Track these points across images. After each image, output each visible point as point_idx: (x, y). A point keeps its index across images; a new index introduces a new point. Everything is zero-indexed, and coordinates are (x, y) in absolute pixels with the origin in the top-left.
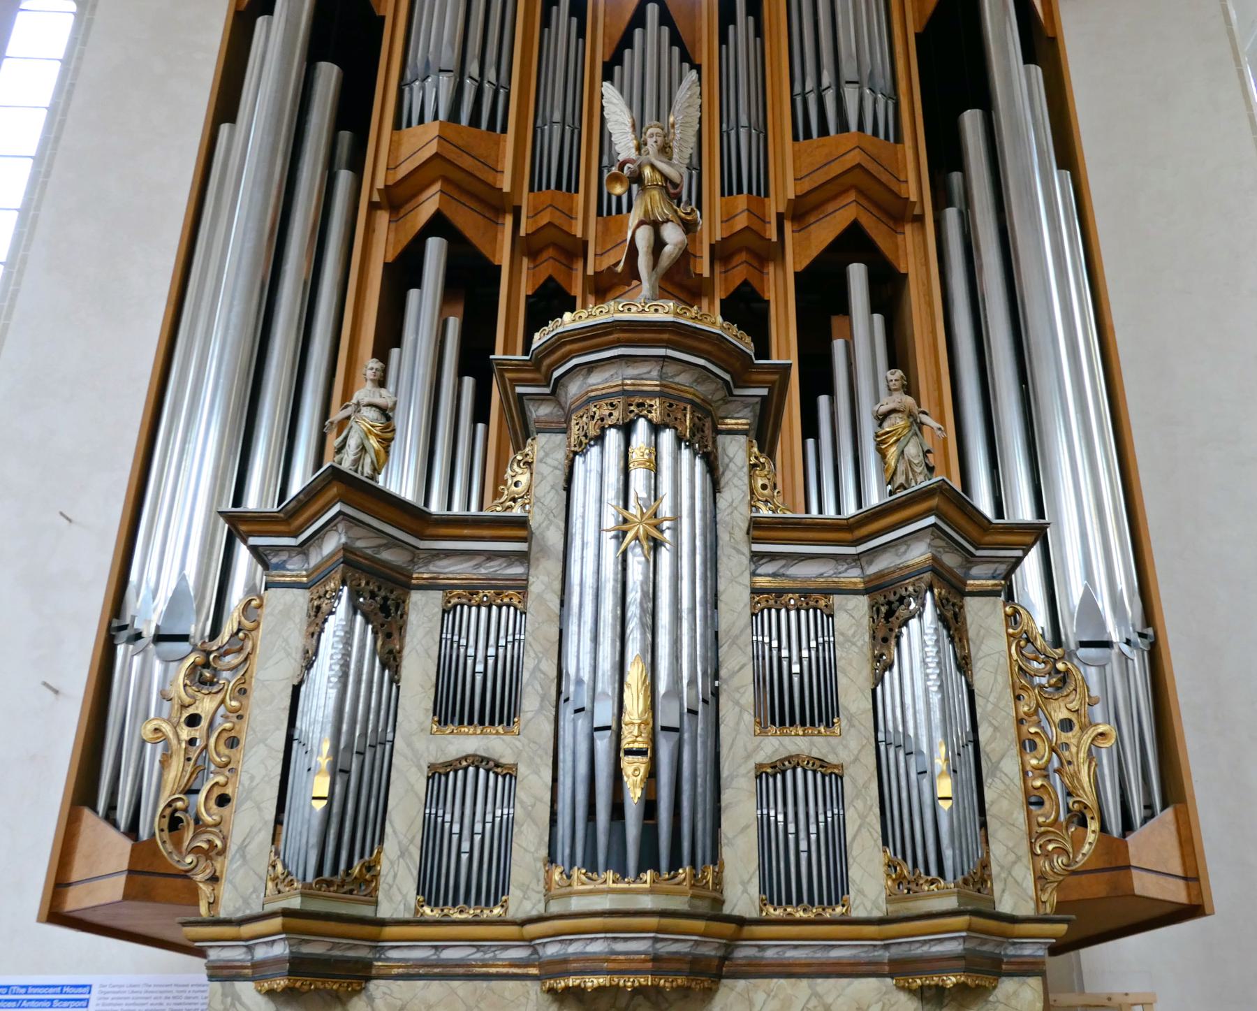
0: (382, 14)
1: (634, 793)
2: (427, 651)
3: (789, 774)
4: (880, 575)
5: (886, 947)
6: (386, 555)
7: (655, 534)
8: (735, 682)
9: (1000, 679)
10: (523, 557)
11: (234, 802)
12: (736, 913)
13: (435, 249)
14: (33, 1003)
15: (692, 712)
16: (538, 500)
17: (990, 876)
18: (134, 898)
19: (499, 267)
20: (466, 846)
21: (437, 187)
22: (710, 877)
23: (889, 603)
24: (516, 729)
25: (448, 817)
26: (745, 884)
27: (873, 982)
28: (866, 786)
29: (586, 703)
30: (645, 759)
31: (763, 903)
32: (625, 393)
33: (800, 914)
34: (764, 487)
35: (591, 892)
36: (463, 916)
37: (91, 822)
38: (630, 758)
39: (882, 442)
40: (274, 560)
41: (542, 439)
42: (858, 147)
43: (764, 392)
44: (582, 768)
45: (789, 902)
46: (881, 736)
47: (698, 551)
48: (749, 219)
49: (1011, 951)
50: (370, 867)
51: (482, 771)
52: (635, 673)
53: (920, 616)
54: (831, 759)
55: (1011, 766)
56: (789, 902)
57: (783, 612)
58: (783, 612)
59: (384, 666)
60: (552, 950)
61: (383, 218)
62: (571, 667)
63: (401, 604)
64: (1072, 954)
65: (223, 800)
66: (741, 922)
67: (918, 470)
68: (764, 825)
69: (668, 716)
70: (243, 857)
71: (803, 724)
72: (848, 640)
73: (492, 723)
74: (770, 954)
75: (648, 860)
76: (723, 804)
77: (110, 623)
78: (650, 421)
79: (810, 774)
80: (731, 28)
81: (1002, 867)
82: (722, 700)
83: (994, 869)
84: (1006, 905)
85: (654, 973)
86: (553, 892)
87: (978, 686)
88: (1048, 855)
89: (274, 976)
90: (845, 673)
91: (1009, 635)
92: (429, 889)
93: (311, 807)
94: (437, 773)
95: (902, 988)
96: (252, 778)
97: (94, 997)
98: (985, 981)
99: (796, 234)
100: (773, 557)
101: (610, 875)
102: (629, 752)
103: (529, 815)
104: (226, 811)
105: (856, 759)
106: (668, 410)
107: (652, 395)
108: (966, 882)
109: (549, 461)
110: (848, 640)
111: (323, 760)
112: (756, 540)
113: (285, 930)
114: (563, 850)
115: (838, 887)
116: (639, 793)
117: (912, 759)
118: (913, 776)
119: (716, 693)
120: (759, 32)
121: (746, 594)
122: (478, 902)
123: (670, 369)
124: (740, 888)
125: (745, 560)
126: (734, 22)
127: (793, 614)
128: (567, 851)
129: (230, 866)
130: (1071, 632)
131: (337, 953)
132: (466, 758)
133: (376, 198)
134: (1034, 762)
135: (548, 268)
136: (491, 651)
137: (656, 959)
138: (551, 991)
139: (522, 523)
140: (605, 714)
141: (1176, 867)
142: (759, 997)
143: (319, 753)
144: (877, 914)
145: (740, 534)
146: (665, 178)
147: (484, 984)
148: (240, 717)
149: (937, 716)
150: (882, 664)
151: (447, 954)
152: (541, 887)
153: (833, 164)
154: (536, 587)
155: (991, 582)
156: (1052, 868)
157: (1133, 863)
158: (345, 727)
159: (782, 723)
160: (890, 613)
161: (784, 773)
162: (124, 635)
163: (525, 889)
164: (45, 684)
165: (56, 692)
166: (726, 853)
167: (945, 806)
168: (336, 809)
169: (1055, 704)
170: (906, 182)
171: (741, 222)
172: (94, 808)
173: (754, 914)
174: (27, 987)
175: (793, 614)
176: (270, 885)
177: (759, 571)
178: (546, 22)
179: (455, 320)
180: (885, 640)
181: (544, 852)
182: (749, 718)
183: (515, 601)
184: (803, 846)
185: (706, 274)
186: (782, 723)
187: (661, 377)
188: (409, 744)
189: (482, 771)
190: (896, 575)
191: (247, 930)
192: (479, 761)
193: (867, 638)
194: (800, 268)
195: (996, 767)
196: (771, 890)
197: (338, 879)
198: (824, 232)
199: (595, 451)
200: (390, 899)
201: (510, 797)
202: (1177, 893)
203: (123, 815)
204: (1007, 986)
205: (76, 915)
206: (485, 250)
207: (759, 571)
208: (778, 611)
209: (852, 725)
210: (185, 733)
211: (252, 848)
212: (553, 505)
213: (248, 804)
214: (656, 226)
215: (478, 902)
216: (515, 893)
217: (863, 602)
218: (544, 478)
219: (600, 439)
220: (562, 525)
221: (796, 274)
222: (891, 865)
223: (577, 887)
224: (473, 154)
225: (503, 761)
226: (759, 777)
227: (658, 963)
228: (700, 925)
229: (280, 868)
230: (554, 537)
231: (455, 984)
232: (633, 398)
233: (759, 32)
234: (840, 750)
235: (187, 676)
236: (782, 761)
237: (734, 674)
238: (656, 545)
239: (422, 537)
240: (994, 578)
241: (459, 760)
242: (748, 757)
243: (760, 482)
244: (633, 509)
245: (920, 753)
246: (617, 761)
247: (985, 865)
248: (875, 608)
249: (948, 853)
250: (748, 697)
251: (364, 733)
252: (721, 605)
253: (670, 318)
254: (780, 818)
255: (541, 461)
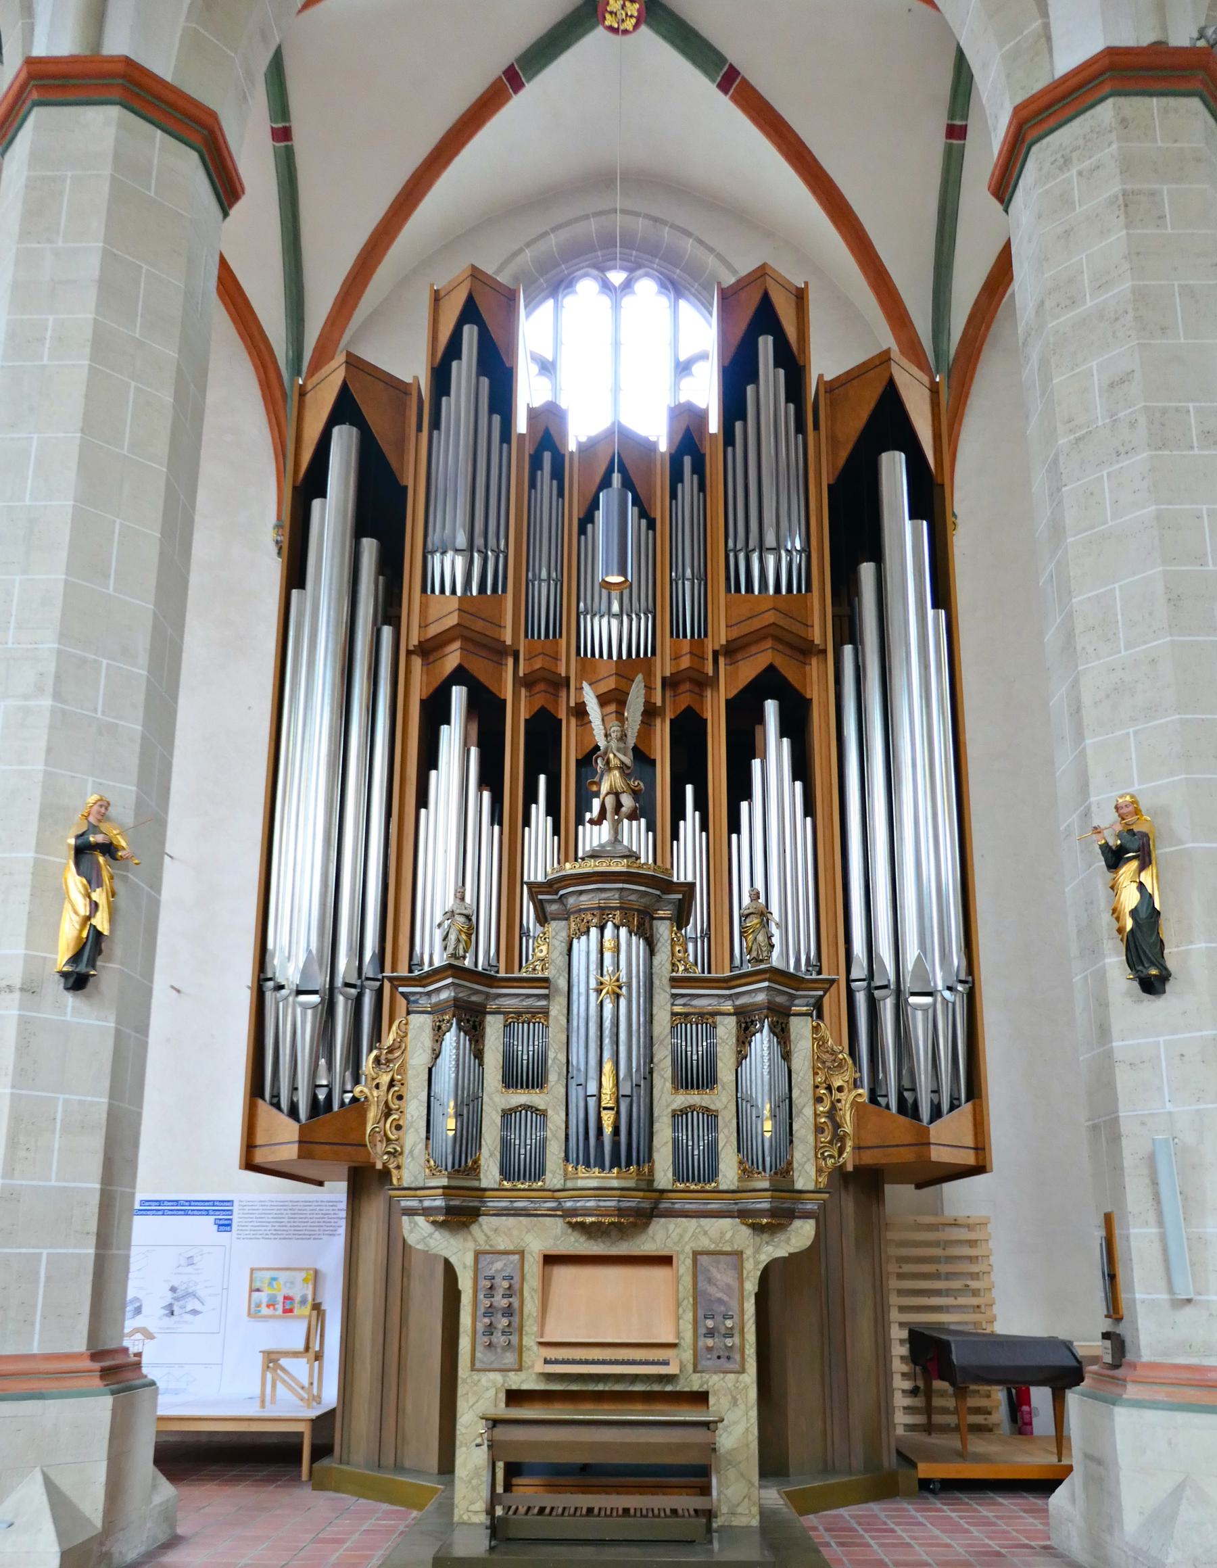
0: (404, 484)
1: (608, 1130)
2: (497, 1048)
3: (690, 1114)
4: (743, 1006)
5: (736, 1204)
6: (474, 998)
7: (617, 990)
8: (662, 1065)
9: (806, 1063)
10: (546, 997)
11: (404, 1129)
12: (660, 1187)
13: (458, 694)
14: (195, 1212)
15: (638, 1086)
16: (553, 961)
17: (792, 1169)
18: (304, 1158)
19: (505, 701)
20: (522, 1151)
21: (457, 645)
22: (646, 1170)
23: (746, 1023)
24: (545, 1090)
25: (513, 1136)
26: (665, 1171)
27: (728, 1220)
28: (730, 1121)
29: (582, 1081)
30: (614, 1112)
31: (674, 1181)
32: (600, 908)
33: (693, 1187)
34: (679, 951)
35: (587, 1178)
36: (522, 1187)
37: (263, 1107)
38: (606, 1112)
39: (745, 932)
40: (412, 998)
41: (554, 924)
42: (774, 608)
43: (680, 896)
44: (582, 1116)
45: (688, 1180)
46: (739, 1095)
47: (642, 995)
48: (691, 660)
49: (800, 1206)
50: (476, 1162)
51: (529, 1113)
52: (608, 1067)
53: (762, 1032)
54: (712, 1107)
55: (808, 1112)
56: (688, 1180)
57: (689, 1025)
58: (689, 1025)
59: (475, 1057)
60: (569, 1204)
61: (417, 662)
62: (574, 1061)
63: (482, 1023)
64: (938, 1186)
65: (399, 1128)
66: (663, 1191)
67: (764, 949)
68: (676, 1142)
69: (625, 1089)
70: (412, 1156)
71: (698, 1088)
72: (723, 1042)
73: (533, 1087)
74: (677, 1206)
75: (615, 1163)
76: (655, 1130)
77: (259, 976)
78: (614, 924)
79: (701, 1115)
80: (680, 485)
81: (799, 1164)
82: (655, 1075)
83: (795, 1165)
84: (799, 1185)
85: (619, 1216)
86: (569, 1176)
87: (793, 1067)
88: (824, 1159)
89: (437, 1215)
90: (721, 1060)
91: (813, 1038)
92: (506, 1172)
93: (447, 1135)
94: (507, 1114)
95: (743, 1224)
96: (412, 1116)
97: (236, 1208)
98: (783, 1221)
99: (728, 667)
100: (683, 996)
101: (597, 1170)
102: (605, 1108)
103: (554, 1136)
104: (400, 1133)
105: (726, 1107)
106: (625, 916)
107: (615, 909)
108: (776, 1173)
109: (558, 937)
110: (723, 1042)
111: (451, 1111)
112: (673, 987)
113: (444, 1195)
114: (572, 1155)
115: (712, 1173)
116: (610, 1129)
117: (754, 1109)
118: (754, 1118)
119: (651, 1072)
120: (702, 488)
121: (668, 1016)
122: (530, 1179)
123: (625, 894)
124: (662, 1174)
125: (668, 997)
126: (682, 481)
127: (694, 1026)
128: (575, 1156)
129: (406, 1161)
130: (908, 983)
131: (464, 1204)
132: (520, 1106)
133: (411, 648)
134: (821, 1109)
135: (540, 701)
136: (531, 1048)
137: (619, 1209)
138: (569, 1223)
139: (546, 980)
140: (592, 1088)
141: (969, 1141)
142: (672, 1227)
143: (448, 1107)
144: (733, 1187)
145: (666, 981)
146: (622, 763)
147: (535, 1219)
148: (402, 1084)
149: (766, 1088)
150: (741, 1057)
151: (516, 1205)
152: (562, 1172)
153: (754, 619)
154: (554, 1012)
155: (805, 1008)
156: (826, 1164)
157: (932, 1141)
158: (460, 1093)
159: (687, 1088)
160: (746, 1029)
161: (687, 1114)
162: (270, 984)
163: (554, 1173)
164: (172, 987)
165: (178, 991)
166: (656, 1156)
167: (768, 1135)
168: (458, 1135)
169: (836, 1077)
170: (813, 626)
171: (685, 662)
172: (263, 1097)
173: (670, 1188)
174: (189, 1201)
175: (694, 1026)
176: (427, 1170)
177: (676, 1003)
178: (533, 485)
179: (461, 692)
180: (743, 1043)
181: (563, 1155)
182: (669, 1085)
183: (542, 1021)
184: (696, 1152)
185: (659, 703)
186: (687, 1088)
187: (620, 898)
188: (491, 1099)
189: (529, 1113)
190: (750, 1008)
191: (419, 1193)
192: (528, 1108)
193: (734, 1040)
194: (730, 696)
195: (800, 1112)
196: (678, 1175)
197: (462, 1168)
198: (749, 669)
199: (584, 938)
200: (487, 1178)
201: (544, 1126)
202: (969, 1159)
203: (284, 1104)
204: (797, 1223)
205: (262, 1165)
206: (494, 689)
207: (676, 1003)
208: (686, 1025)
209: (724, 1089)
210: (375, 1093)
211: (416, 1152)
212: (561, 964)
213: (412, 1130)
214: (617, 795)
215: (530, 1179)
216: (548, 1175)
217: (733, 1019)
218: (555, 948)
219: (587, 932)
220: (567, 976)
221: (727, 701)
222: (741, 1163)
223: (581, 1175)
224: (483, 616)
225: (540, 1108)
226: (674, 1116)
227: (621, 1212)
228: (641, 1194)
229: (432, 1163)
230: (562, 983)
231: (521, 1218)
232: (603, 912)
233: (702, 488)
234: (717, 1102)
235: (373, 1062)
236: (686, 1108)
237: (661, 1061)
238: (618, 996)
239: (491, 987)
240: (807, 1006)
241: (517, 1107)
242: (668, 1106)
243: (677, 948)
244: (606, 978)
245: (757, 1106)
246: (599, 1113)
247: (790, 1163)
248: (739, 1023)
249: (768, 1159)
250: (668, 1073)
251: (468, 1095)
252: (654, 1022)
253: (624, 869)
254: (684, 1137)
255: (553, 938)
